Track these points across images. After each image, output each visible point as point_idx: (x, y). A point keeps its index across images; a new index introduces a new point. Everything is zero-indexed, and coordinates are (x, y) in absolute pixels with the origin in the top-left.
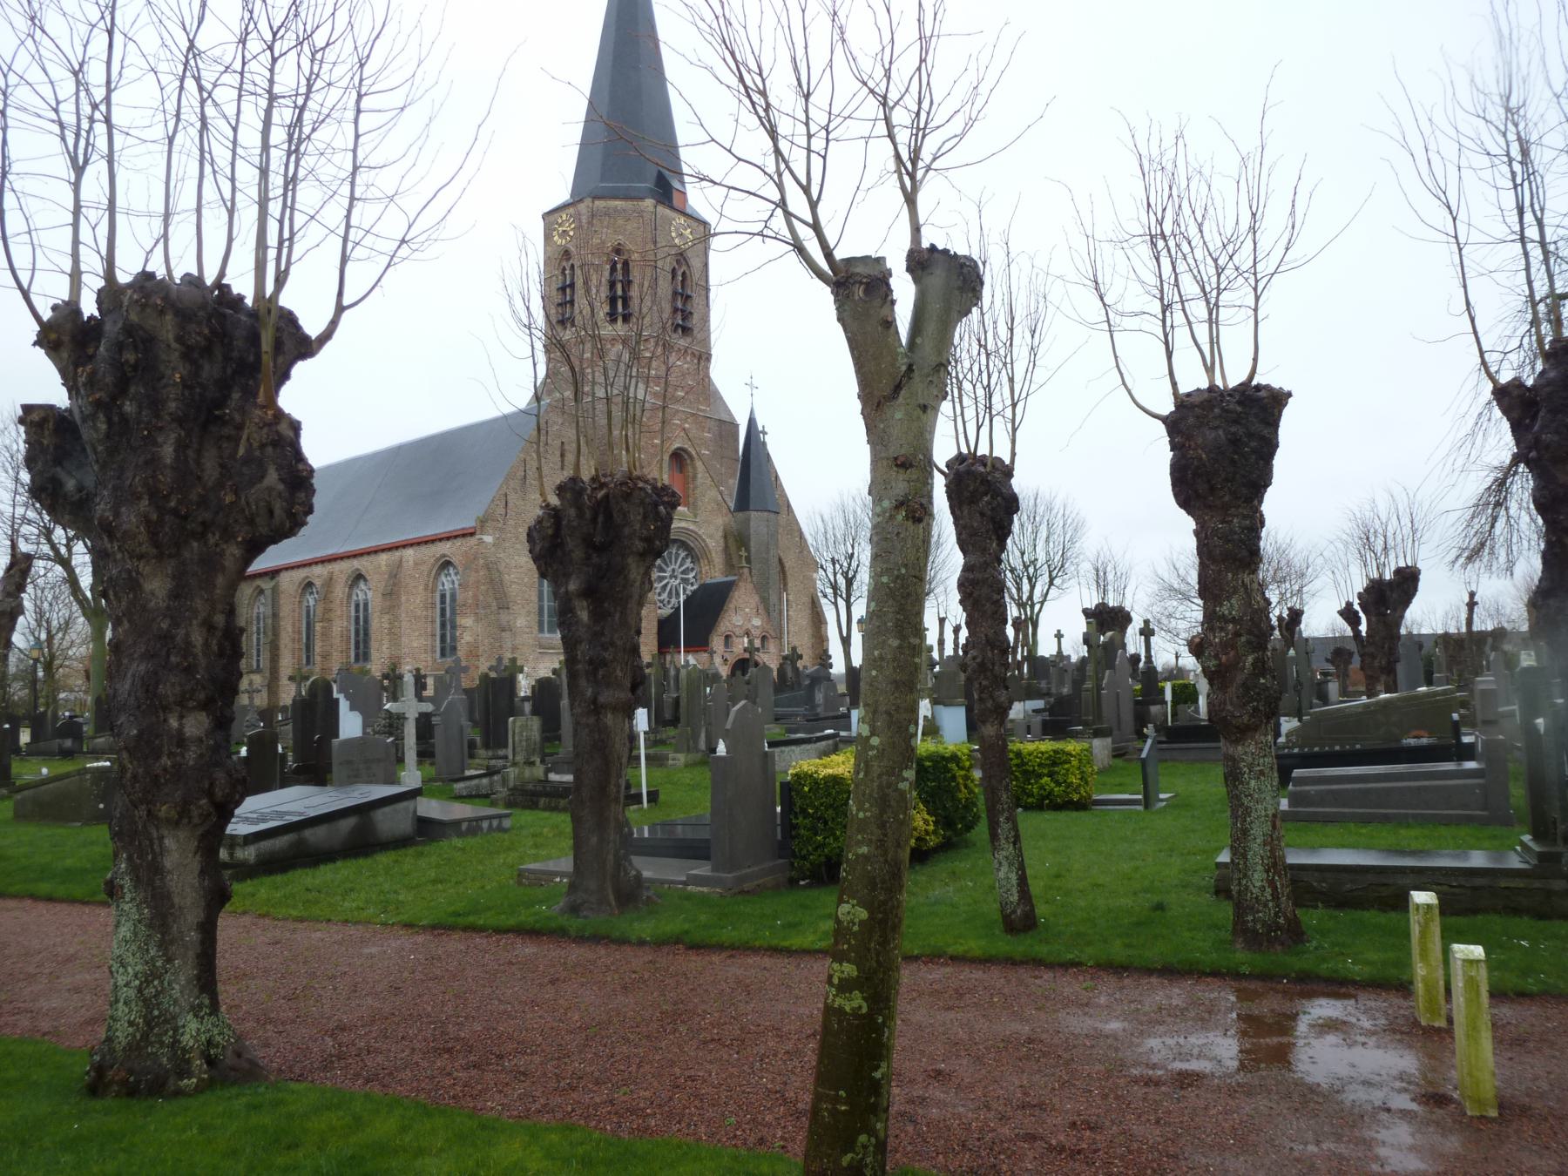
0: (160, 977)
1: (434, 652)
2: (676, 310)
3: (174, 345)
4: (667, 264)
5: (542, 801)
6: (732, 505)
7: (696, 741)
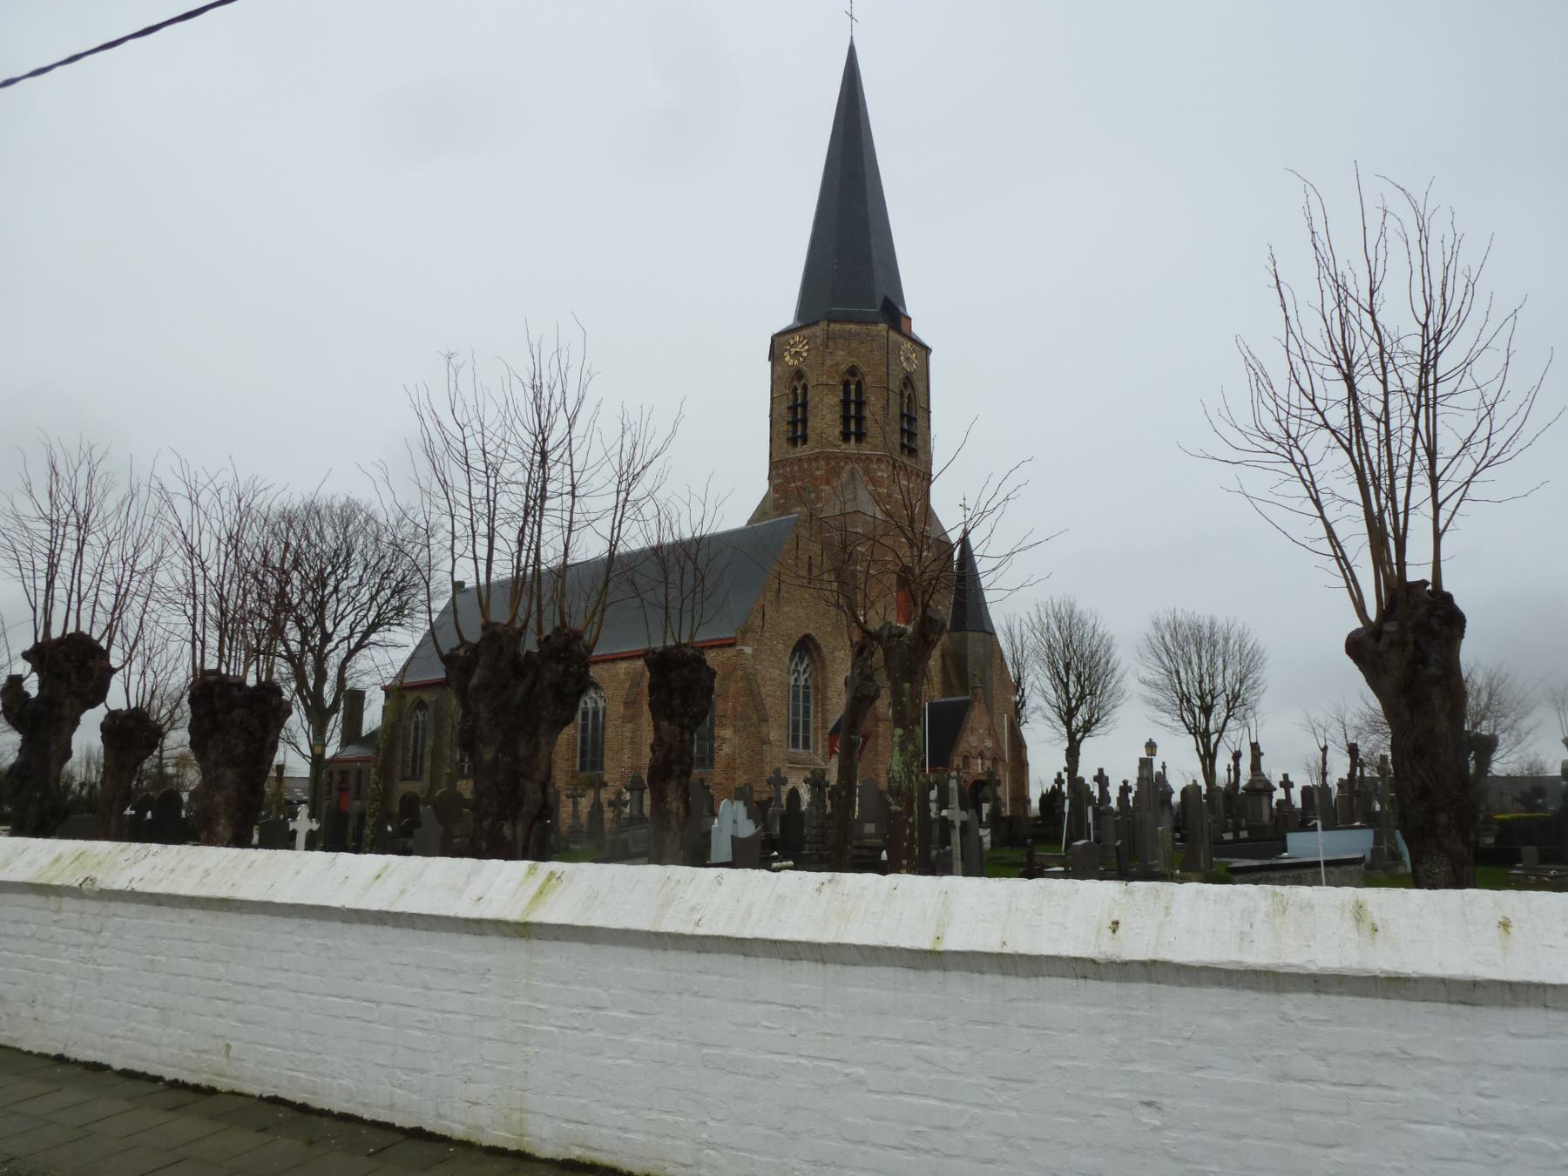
2: (902, 430)
4: (895, 385)
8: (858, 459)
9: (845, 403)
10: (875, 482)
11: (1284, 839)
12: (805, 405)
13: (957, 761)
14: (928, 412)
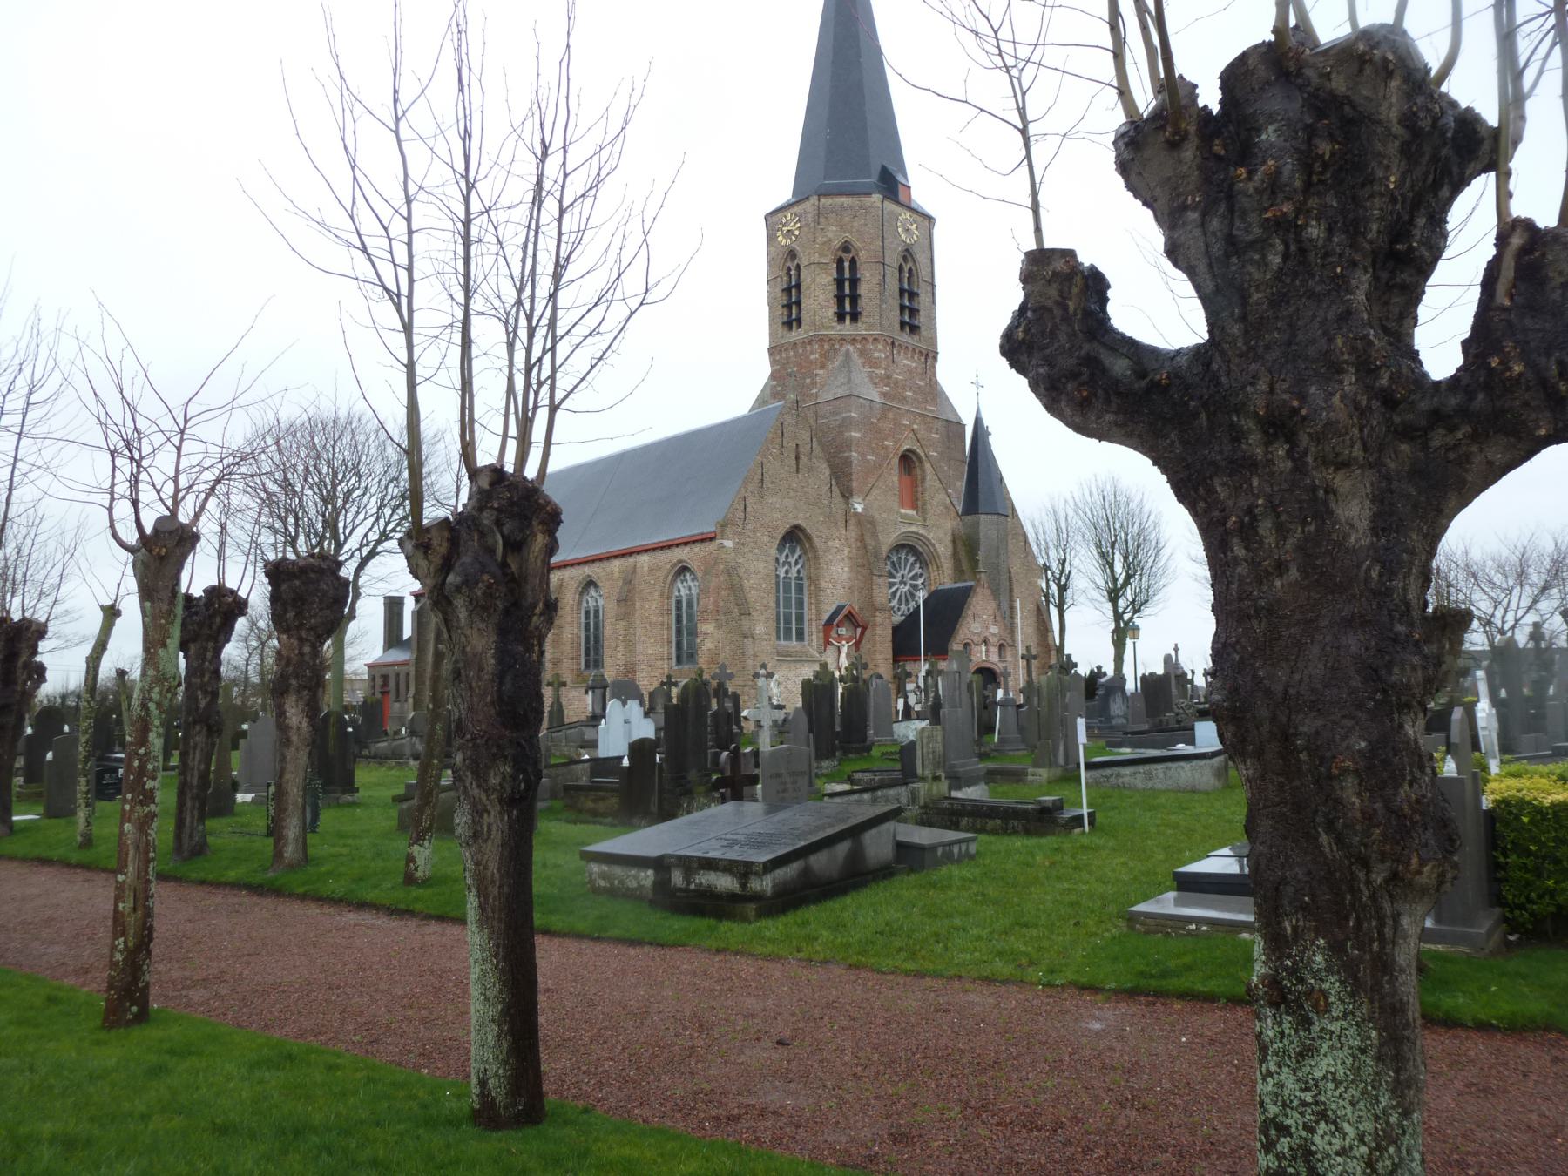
0: (1395, 1141)
1: (670, 659)
2: (902, 308)
3: (1396, 129)
4: (893, 259)
5: (964, 821)
6: (960, 509)
7: (1056, 756)
8: (854, 341)
9: (840, 282)
10: (873, 363)
11: (1192, 729)
12: (798, 286)
13: (956, 646)
14: (933, 286)
